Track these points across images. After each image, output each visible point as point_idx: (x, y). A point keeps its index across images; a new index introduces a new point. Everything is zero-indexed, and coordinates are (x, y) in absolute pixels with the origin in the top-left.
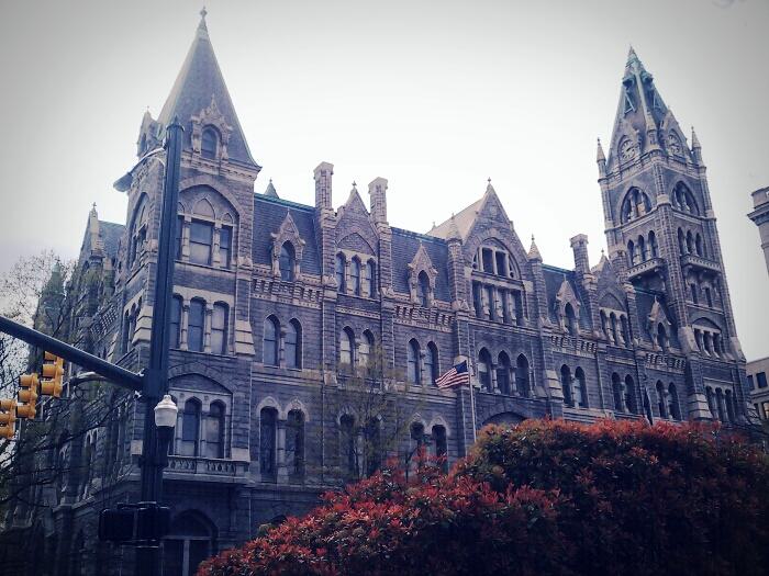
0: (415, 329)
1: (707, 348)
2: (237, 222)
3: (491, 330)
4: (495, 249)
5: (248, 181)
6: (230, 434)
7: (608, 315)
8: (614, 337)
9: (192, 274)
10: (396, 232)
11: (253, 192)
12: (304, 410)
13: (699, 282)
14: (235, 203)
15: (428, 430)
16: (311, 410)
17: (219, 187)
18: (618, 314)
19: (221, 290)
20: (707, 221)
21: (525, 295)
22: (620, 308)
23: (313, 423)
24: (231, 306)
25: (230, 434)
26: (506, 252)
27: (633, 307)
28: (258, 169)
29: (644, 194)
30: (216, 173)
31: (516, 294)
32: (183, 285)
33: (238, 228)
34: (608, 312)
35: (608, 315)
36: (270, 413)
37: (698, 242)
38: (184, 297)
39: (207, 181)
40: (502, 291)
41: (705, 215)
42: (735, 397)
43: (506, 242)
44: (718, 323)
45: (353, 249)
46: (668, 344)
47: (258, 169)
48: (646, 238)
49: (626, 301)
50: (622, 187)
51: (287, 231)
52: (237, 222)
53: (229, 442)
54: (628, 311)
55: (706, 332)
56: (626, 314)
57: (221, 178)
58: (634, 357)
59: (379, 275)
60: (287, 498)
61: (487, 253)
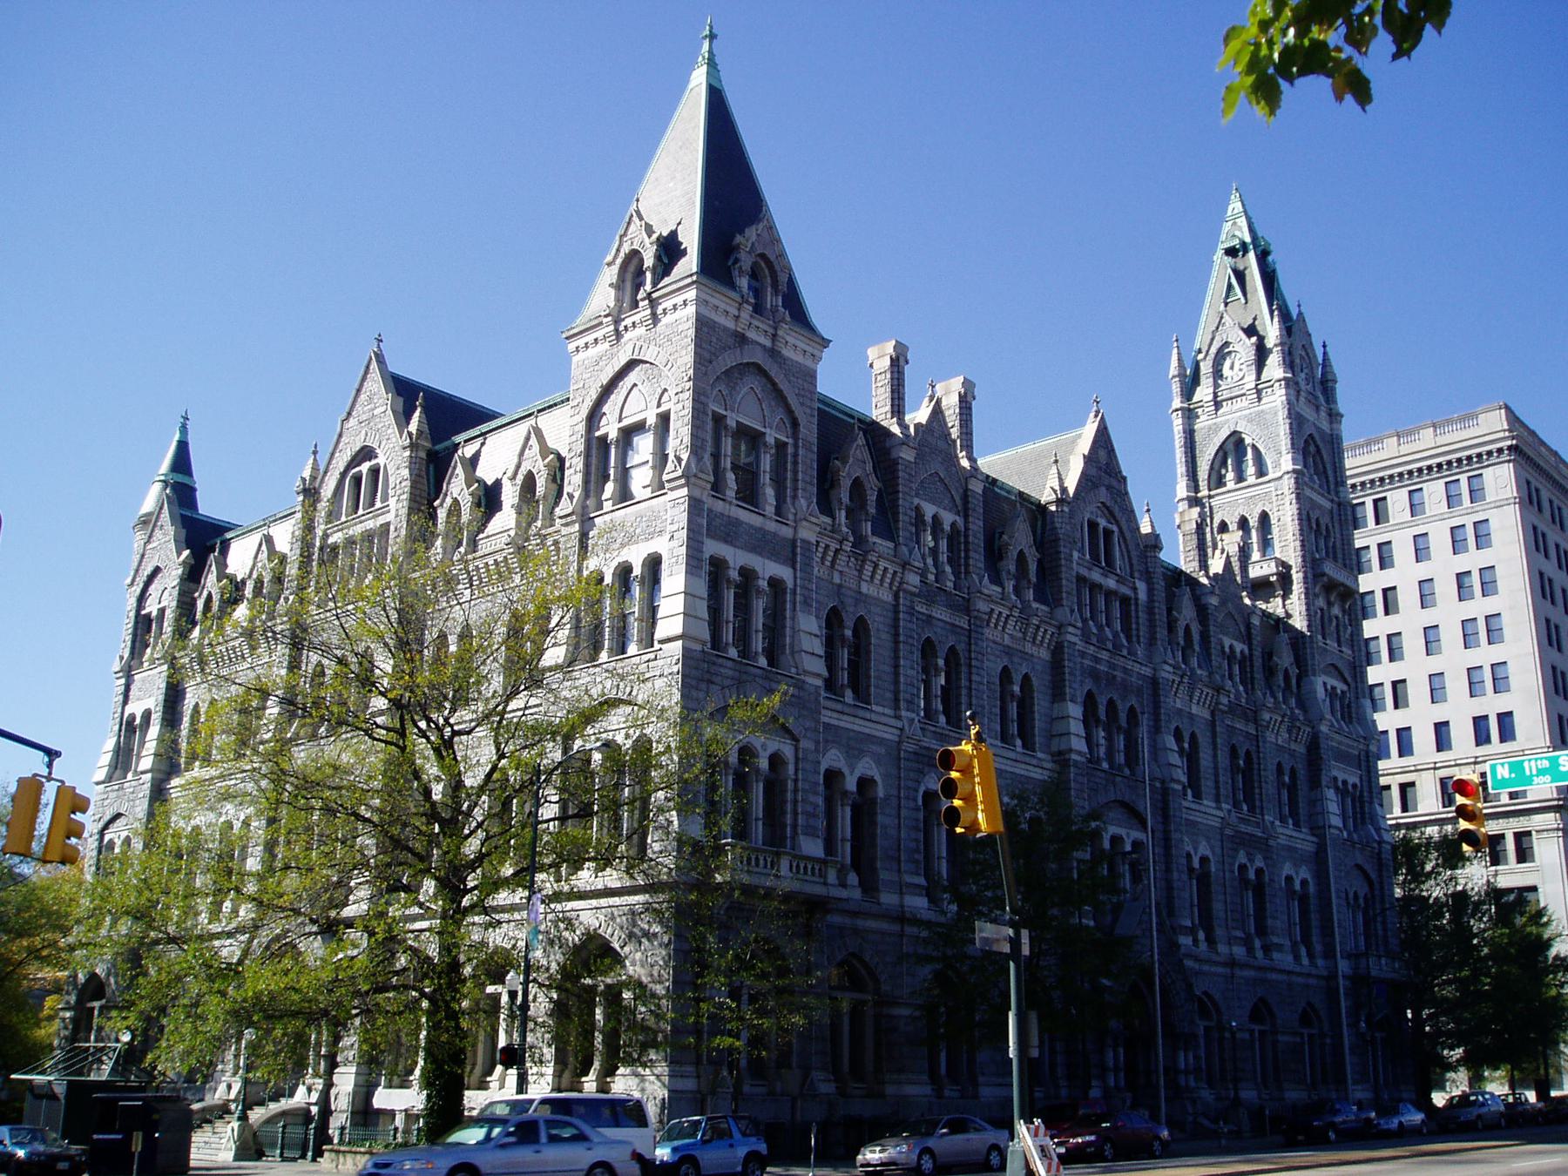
0: (1008, 652)
1: (1231, 678)
2: (795, 436)
3: (1097, 660)
4: (1102, 523)
5: (809, 363)
6: (795, 813)
7: (928, 518)
8: (936, 564)
9: (737, 523)
10: (824, 400)
11: (813, 391)
12: (878, 778)
13: (1330, 604)
14: (793, 401)
15: (851, 784)
16: (885, 776)
17: (768, 364)
18: (948, 518)
19: (774, 555)
20: (1339, 504)
21: (1137, 604)
22: (953, 508)
23: (887, 798)
24: (790, 584)
25: (795, 813)
26: (1115, 528)
27: (1257, 639)
28: (825, 343)
29: (1254, 447)
30: (768, 343)
31: (1125, 601)
32: (726, 542)
33: (796, 446)
34: (929, 510)
35: (928, 518)
36: (833, 776)
37: (1327, 537)
38: (731, 564)
39: (759, 358)
40: (1109, 594)
41: (1337, 493)
42: (1361, 796)
43: (1118, 514)
44: (1347, 675)
45: (933, 501)
46: (1030, 594)
47: (825, 343)
48: (1253, 522)
49: (1248, 626)
50: (1218, 428)
51: (1020, 538)
52: (795, 436)
53: (795, 826)
54: (966, 517)
55: (935, 517)
56: (960, 521)
57: (773, 353)
58: (1256, 721)
59: (967, 551)
60: (860, 923)
61: (1093, 525)
